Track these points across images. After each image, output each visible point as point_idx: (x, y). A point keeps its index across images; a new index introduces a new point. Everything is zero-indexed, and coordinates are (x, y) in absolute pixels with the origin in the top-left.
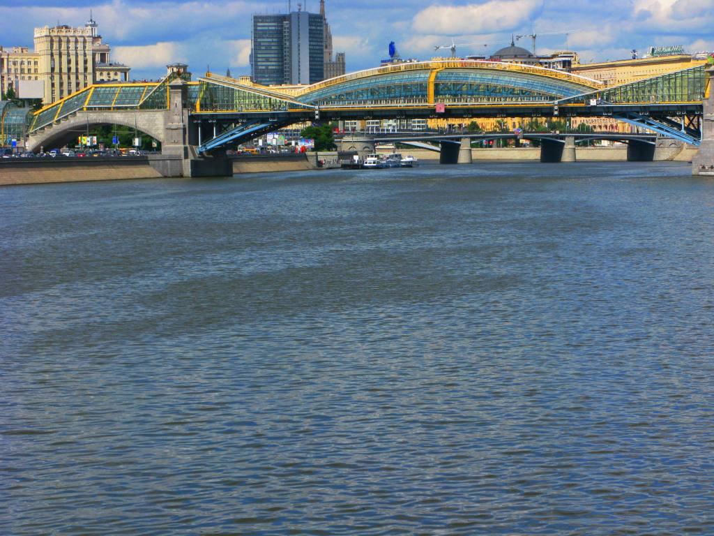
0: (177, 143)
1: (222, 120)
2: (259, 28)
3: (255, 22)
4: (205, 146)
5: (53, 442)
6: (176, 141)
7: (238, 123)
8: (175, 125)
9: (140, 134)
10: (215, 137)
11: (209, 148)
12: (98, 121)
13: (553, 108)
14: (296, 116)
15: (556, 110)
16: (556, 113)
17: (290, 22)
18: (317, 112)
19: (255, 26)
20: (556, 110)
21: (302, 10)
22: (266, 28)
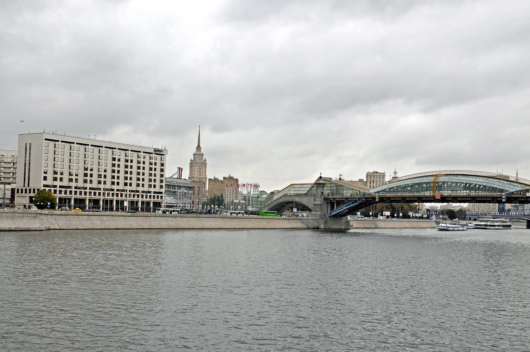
11: (332, 215)
13: (502, 197)
15: (504, 199)
18: (504, 197)
20: (504, 199)
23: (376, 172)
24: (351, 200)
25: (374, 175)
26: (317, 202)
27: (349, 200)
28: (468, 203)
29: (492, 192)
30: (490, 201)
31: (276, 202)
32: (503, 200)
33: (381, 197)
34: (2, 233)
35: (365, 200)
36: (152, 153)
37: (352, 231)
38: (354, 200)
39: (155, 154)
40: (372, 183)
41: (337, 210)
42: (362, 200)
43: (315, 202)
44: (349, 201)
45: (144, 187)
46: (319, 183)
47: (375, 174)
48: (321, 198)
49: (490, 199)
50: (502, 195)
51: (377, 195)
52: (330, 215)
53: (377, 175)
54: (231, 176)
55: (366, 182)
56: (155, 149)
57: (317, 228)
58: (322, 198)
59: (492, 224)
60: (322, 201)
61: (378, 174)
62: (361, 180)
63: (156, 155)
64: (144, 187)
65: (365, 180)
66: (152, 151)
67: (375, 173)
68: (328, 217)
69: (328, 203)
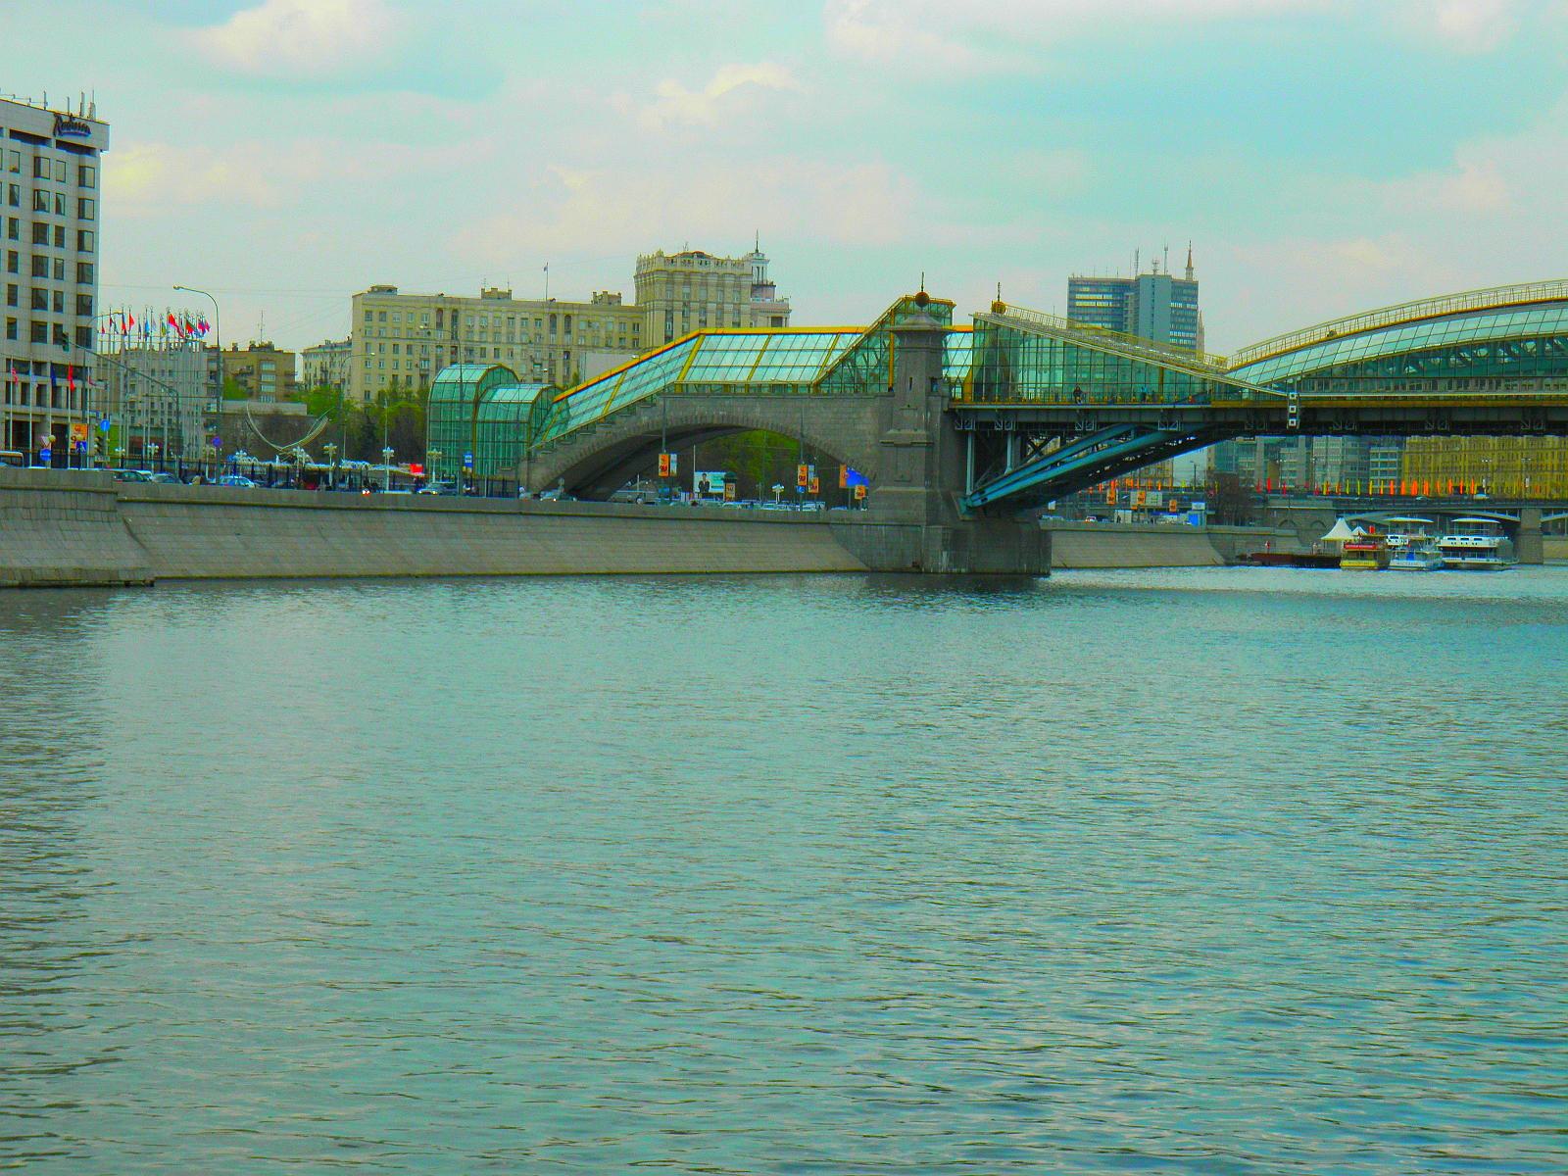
0: (910, 482)
1: (1029, 425)
2: (1078, 304)
3: (1070, 292)
4: (982, 492)
5: (75, 1109)
6: (907, 478)
7: (1072, 434)
8: (907, 433)
9: (809, 453)
10: (1008, 470)
11: (990, 498)
12: (709, 421)
13: (1286, 409)
14: (1232, 418)
15: (1293, 416)
16: (1293, 422)
17: (1137, 294)
18: (1292, 409)
19: (1072, 299)
20: (1293, 416)
21: (1159, 273)
22: (1093, 304)
23: (700, 255)
24: (1113, 419)
25: (687, 269)
26: (903, 432)
27: (1103, 419)
28: (1206, 448)
29: (1483, 384)
30: (1515, 423)
31: (614, 429)
32: (1293, 422)
33: (1311, 404)
34: (4, 591)
35: (1201, 420)
36: (43, 141)
37: (1057, 578)
38: (1135, 419)
39: (60, 145)
40: (678, 316)
41: (1021, 475)
42: (1185, 419)
43: (891, 432)
44: (1102, 425)
45: (14, 338)
46: (915, 327)
47: (697, 268)
48: (928, 407)
49: (1517, 417)
50: (1285, 399)
51: (1293, 395)
52: (979, 503)
53: (703, 269)
54: (488, 289)
55: (639, 311)
56: (57, 116)
57: (917, 569)
58: (939, 407)
59: (1464, 544)
60: (937, 425)
61: (712, 268)
62: (607, 302)
63: (62, 154)
64: (14, 338)
65: (629, 300)
66: (45, 129)
67: (696, 261)
68: (964, 509)
69: (963, 436)
